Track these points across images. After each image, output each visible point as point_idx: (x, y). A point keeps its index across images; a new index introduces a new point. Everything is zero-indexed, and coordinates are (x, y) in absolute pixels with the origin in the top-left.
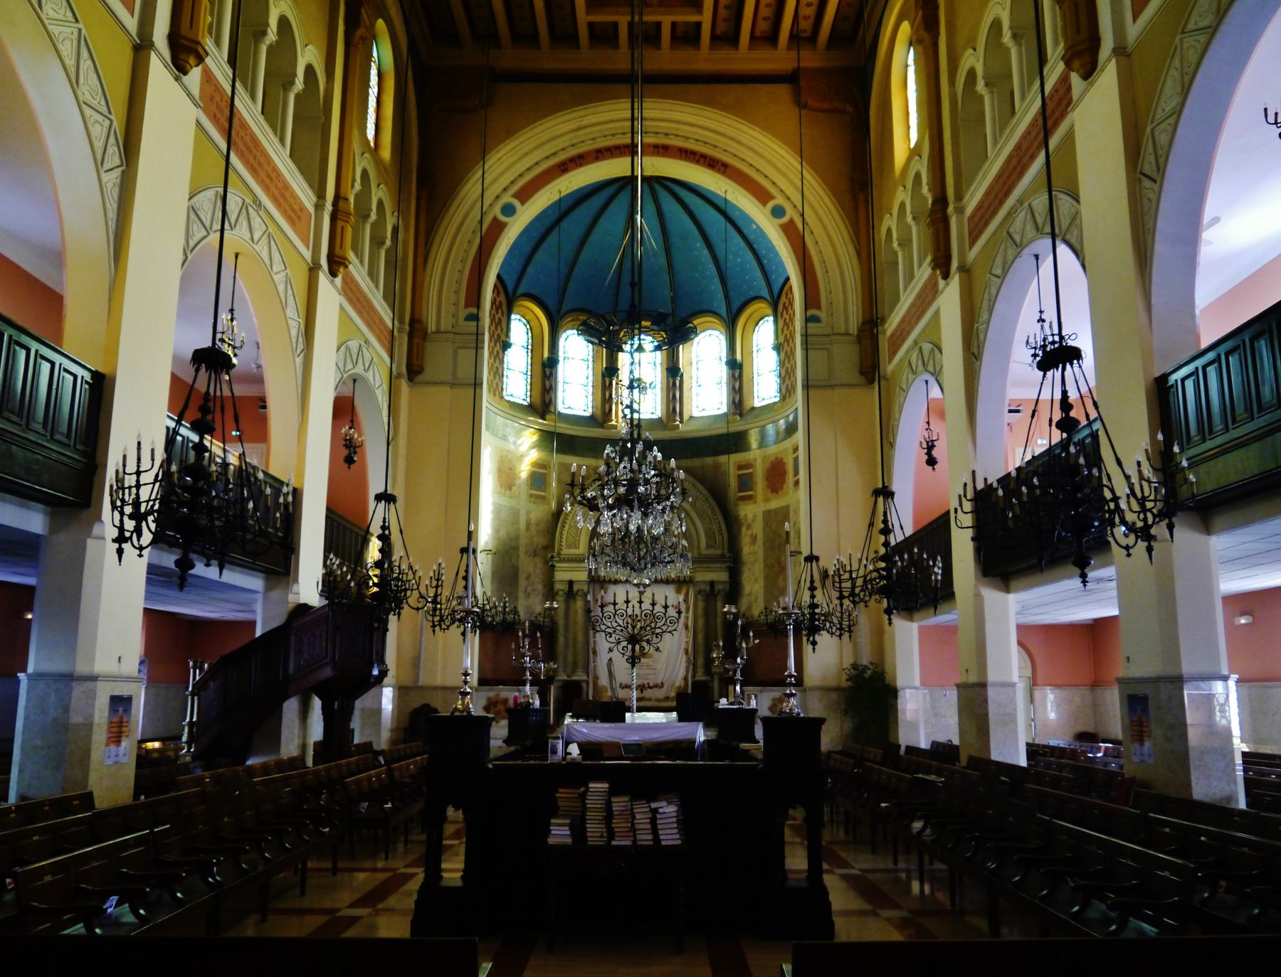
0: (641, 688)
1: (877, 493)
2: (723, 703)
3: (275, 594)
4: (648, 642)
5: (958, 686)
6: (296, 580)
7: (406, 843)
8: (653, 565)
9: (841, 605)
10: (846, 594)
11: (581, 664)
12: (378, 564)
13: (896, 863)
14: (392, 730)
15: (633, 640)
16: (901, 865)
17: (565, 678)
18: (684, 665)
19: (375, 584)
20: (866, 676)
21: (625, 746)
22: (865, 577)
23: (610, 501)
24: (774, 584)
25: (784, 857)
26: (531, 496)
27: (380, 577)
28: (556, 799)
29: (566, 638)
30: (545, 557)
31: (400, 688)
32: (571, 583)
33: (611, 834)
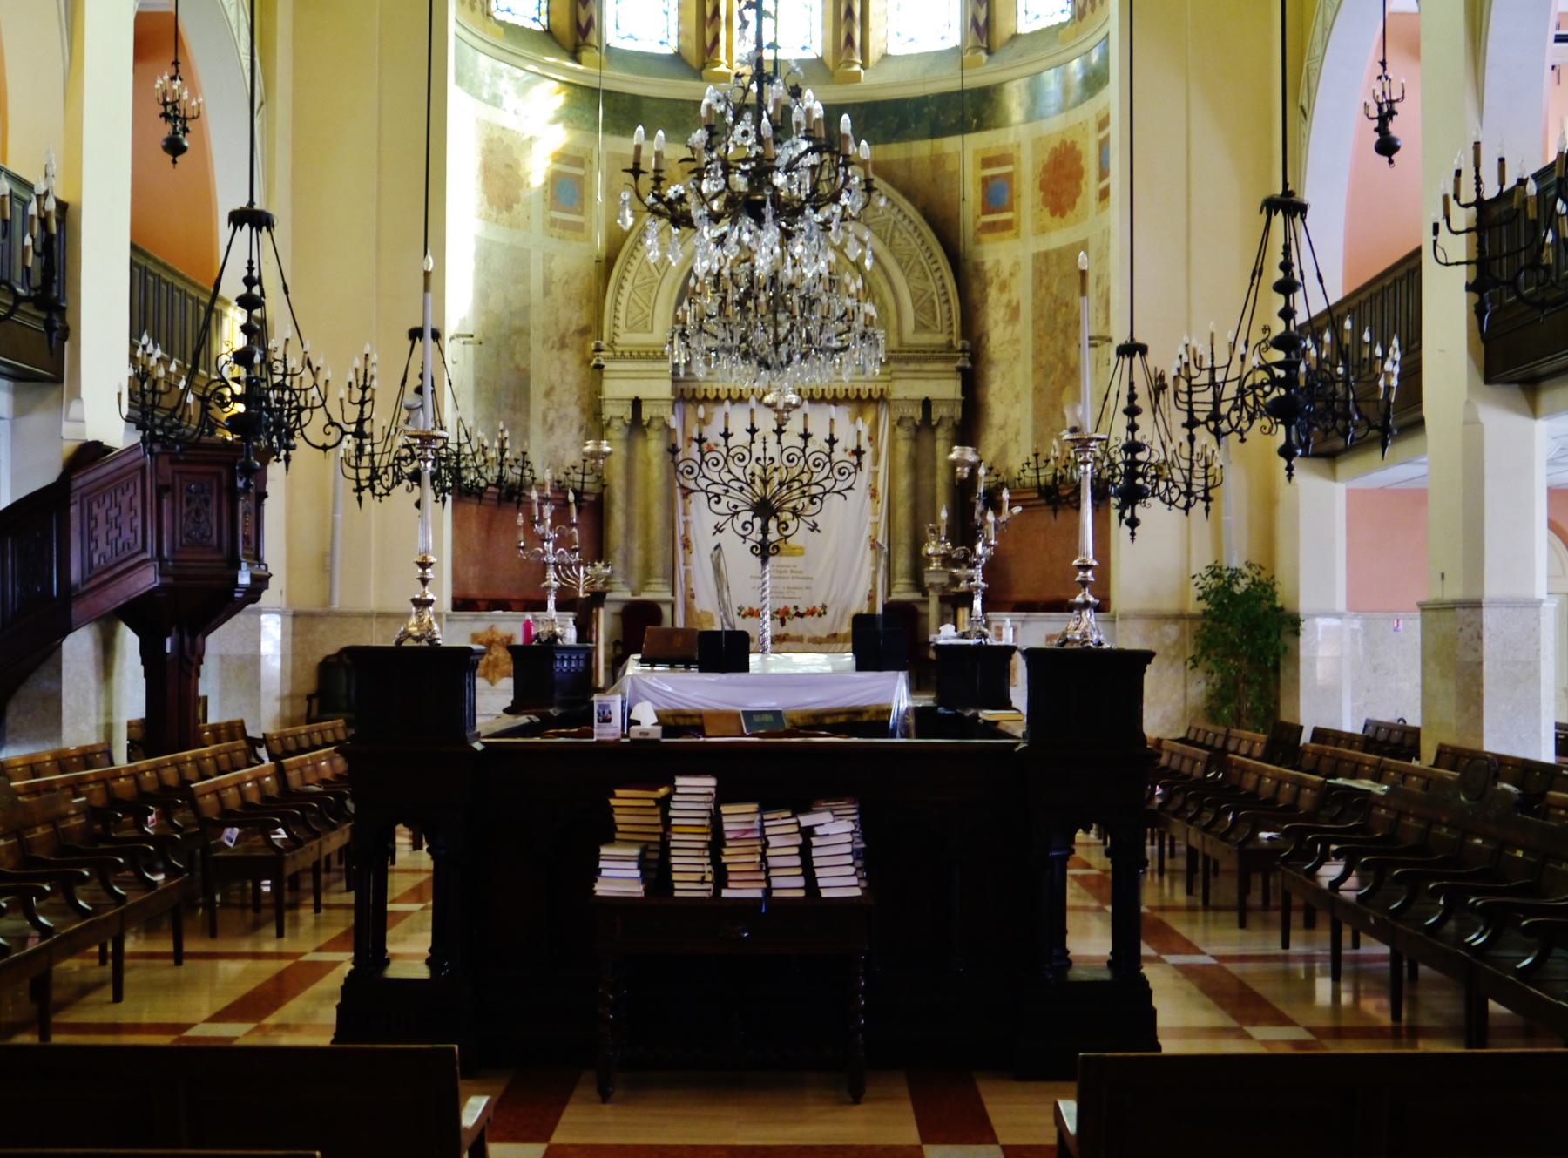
0: (782, 616)
1: (1271, 205)
2: (946, 635)
3: (37, 420)
4: (796, 513)
5: (1424, 608)
6: (76, 394)
7: (317, 907)
8: (804, 356)
9: (1191, 439)
10: (1201, 417)
11: (658, 569)
12: (242, 357)
13: (1286, 945)
14: (282, 699)
15: (764, 509)
16: (1296, 948)
17: (628, 596)
18: (868, 569)
19: (236, 398)
20: (1238, 590)
21: (748, 715)
22: (1241, 379)
23: (716, 205)
24: (1056, 377)
25: (1063, 932)
26: (553, 222)
27: (249, 383)
28: (611, 809)
29: (628, 514)
30: (582, 349)
31: (295, 615)
32: (637, 403)
33: (721, 876)
